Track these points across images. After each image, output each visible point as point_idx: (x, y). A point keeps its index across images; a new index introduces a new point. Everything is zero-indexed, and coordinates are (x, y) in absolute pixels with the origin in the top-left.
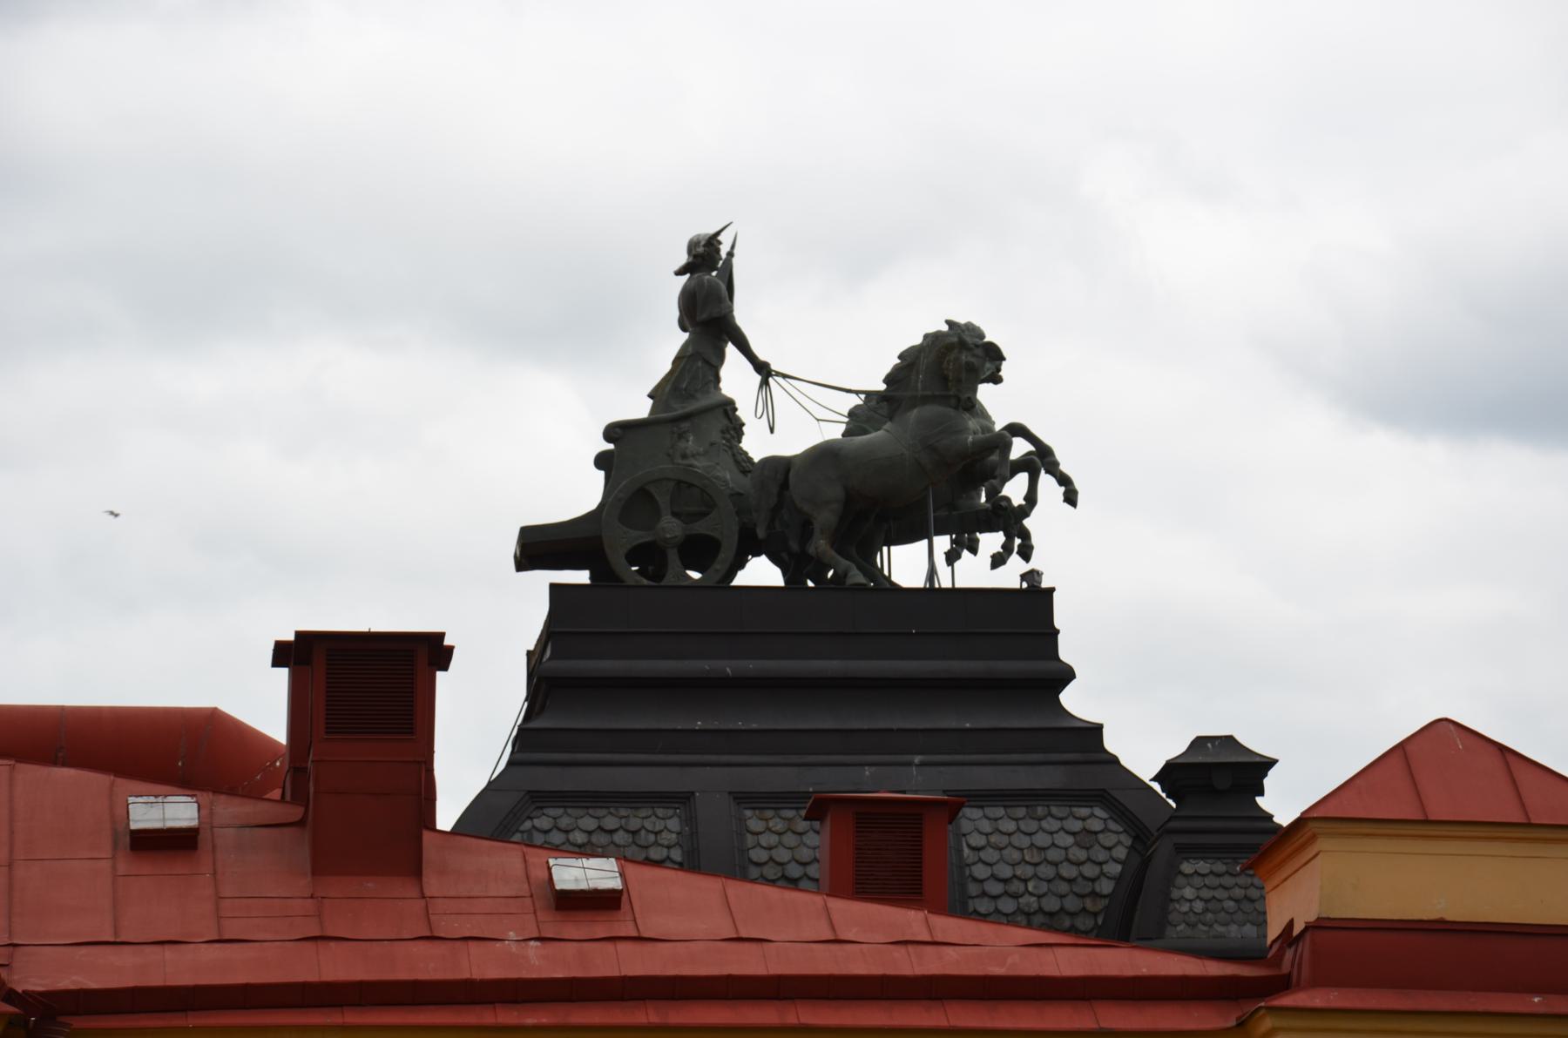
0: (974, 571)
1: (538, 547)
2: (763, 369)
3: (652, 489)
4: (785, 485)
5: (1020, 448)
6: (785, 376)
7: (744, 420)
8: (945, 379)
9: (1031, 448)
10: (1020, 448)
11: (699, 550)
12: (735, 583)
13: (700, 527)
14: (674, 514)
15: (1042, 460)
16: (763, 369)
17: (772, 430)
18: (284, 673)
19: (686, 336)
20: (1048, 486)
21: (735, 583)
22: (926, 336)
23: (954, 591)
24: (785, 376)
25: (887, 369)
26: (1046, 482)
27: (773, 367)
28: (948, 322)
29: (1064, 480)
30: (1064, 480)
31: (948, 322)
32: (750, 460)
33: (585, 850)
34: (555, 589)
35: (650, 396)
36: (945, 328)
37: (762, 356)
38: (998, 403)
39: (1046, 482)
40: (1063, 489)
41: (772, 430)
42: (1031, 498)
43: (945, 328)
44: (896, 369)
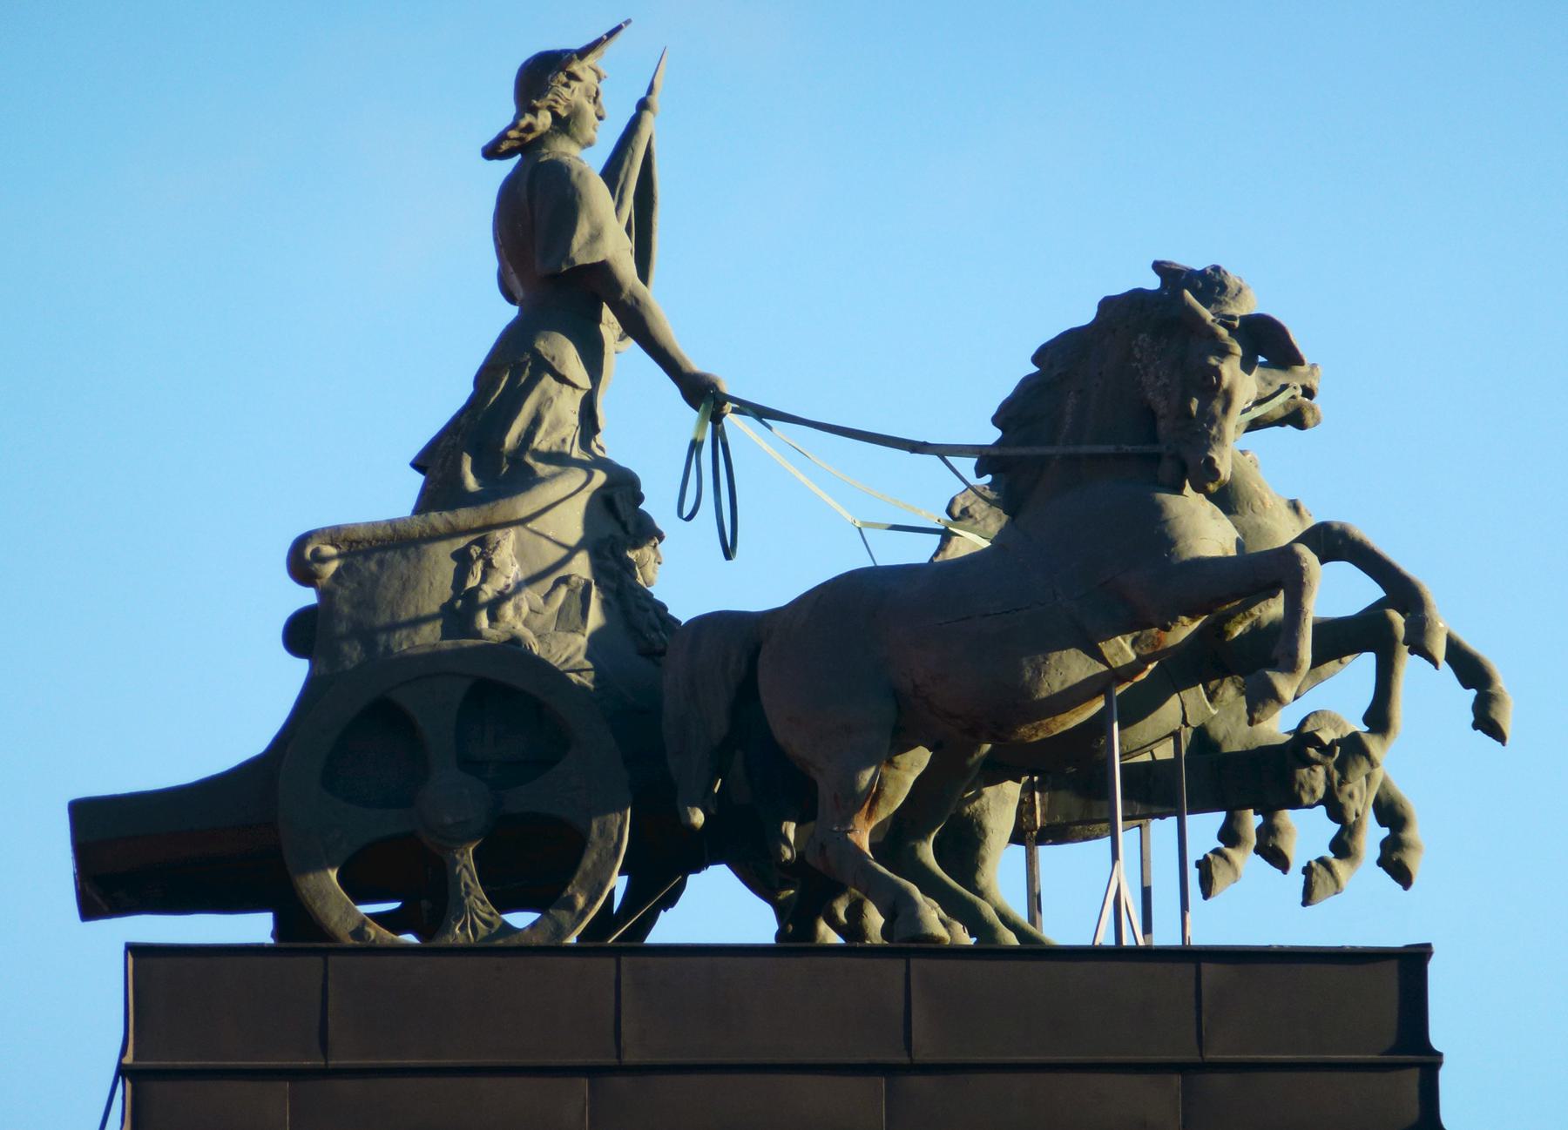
0: (1255, 909)
1: (127, 852)
2: (701, 392)
4: (747, 692)
5: (1337, 591)
6: (762, 414)
8: (1150, 415)
11: (535, 863)
12: (655, 937)
15: (1393, 623)
16: (701, 392)
17: (729, 553)
18: (299, 669)
20: (1425, 687)
21: (655, 937)
22: (1107, 304)
23: (1187, 955)
24: (762, 414)
25: (1005, 389)
27: (727, 388)
28: (1159, 267)
29: (1470, 669)
30: (1470, 669)
31: (1159, 267)
32: (677, 622)
34: (136, 951)
35: (418, 465)
36: (1153, 282)
37: (697, 362)
38: (1272, 476)
40: (1473, 692)
41: (729, 553)
42: (1379, 717)
43: (1153, 282)
44: (1027, 387)
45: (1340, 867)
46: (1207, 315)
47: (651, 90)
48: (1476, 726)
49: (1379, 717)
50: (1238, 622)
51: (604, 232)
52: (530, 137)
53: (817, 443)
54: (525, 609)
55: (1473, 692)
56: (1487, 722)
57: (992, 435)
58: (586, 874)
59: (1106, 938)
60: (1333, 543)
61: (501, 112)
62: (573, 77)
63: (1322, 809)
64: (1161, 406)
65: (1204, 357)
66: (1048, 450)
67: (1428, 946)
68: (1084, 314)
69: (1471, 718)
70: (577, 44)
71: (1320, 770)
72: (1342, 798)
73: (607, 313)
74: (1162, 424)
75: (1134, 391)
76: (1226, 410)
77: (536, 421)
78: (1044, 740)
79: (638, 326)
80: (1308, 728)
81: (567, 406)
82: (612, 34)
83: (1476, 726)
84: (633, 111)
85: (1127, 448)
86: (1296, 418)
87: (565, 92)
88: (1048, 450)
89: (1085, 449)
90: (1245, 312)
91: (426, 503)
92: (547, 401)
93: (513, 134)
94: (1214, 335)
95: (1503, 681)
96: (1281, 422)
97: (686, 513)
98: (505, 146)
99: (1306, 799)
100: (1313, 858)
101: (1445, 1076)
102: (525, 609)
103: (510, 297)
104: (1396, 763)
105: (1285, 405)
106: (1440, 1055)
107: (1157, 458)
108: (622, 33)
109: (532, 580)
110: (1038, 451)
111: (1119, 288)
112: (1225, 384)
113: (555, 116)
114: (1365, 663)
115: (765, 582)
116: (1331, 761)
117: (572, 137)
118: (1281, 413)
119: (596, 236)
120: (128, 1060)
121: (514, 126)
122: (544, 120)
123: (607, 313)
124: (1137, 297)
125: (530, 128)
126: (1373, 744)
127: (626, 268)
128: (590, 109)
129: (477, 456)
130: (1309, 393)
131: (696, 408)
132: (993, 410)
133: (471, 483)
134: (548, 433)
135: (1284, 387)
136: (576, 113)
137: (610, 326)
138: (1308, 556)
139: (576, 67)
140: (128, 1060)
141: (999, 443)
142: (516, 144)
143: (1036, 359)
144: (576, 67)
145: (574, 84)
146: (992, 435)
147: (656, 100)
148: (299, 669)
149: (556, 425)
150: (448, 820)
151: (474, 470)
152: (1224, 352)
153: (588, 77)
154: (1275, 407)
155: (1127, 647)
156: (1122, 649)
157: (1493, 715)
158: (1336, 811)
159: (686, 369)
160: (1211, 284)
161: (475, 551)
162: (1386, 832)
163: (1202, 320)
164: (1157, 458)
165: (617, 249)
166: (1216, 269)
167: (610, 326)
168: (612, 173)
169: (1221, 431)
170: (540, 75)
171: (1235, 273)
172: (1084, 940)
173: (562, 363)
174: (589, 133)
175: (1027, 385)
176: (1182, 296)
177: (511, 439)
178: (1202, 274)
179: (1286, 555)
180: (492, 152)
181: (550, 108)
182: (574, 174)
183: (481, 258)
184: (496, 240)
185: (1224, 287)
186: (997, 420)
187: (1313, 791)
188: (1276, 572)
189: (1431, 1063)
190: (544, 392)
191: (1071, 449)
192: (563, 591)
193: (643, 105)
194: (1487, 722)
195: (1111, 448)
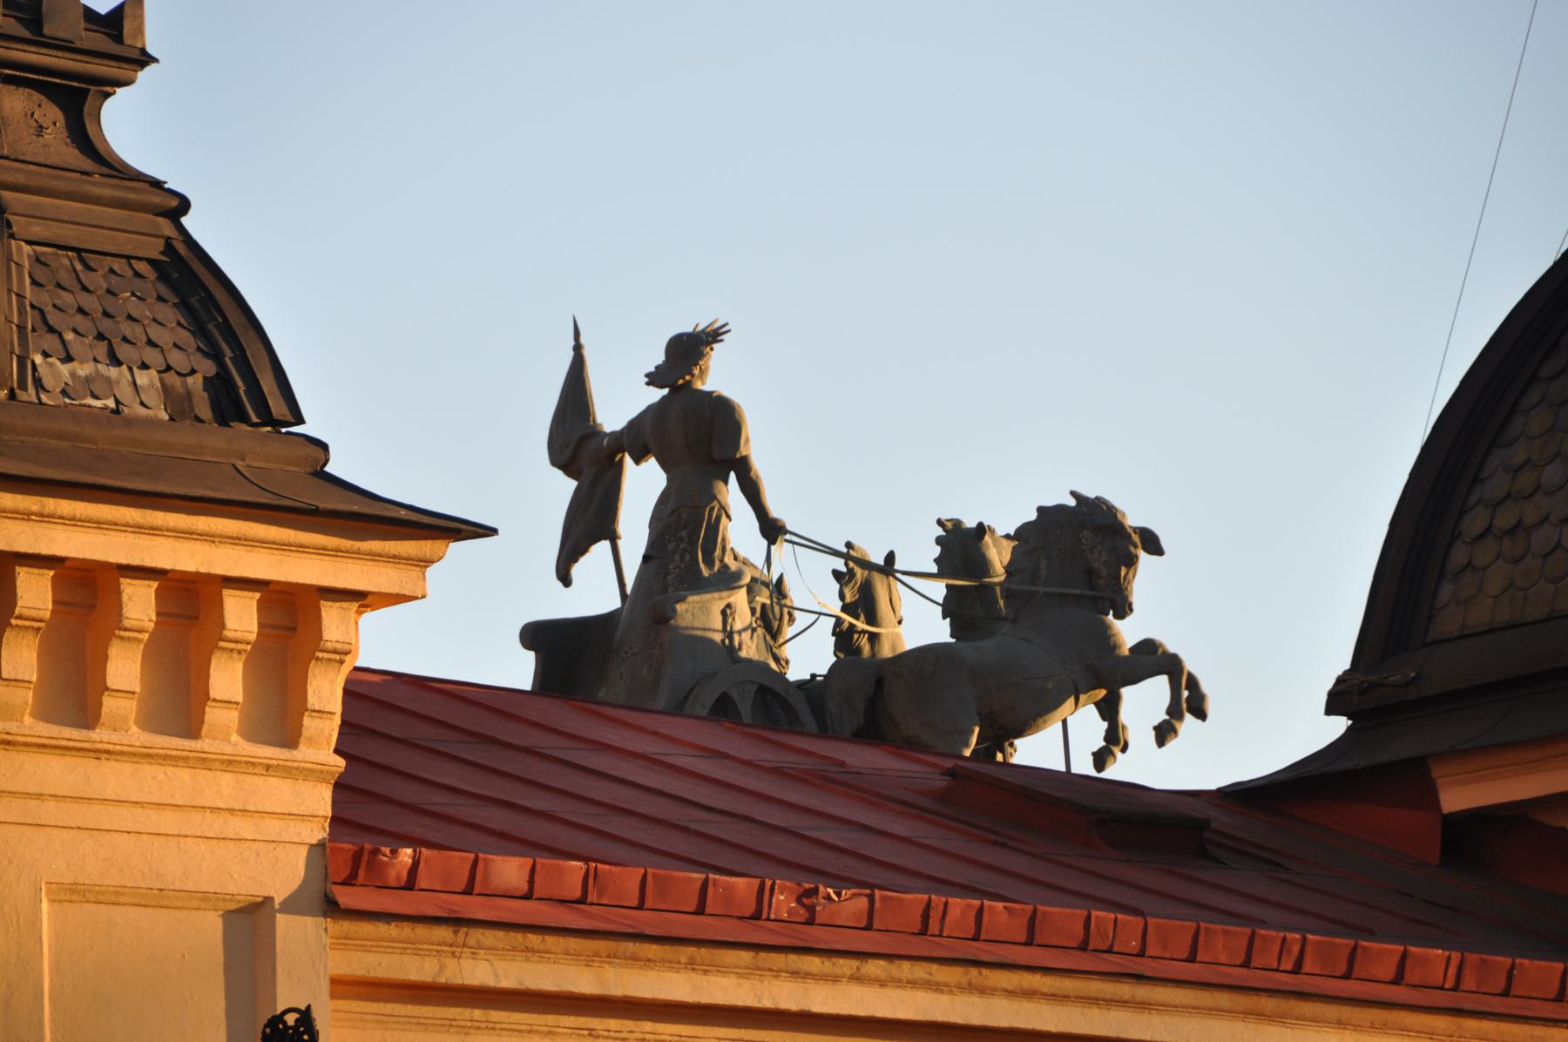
8: (1090, 574)
31: (1073, 494)
36: (1072, 502)
37: (775, 510)
40: (1105, 725)
89: (1053, 590)
111: (1050, 502)
124: (1060, 509)
152: (1136, 547)
164: (1093, 599)
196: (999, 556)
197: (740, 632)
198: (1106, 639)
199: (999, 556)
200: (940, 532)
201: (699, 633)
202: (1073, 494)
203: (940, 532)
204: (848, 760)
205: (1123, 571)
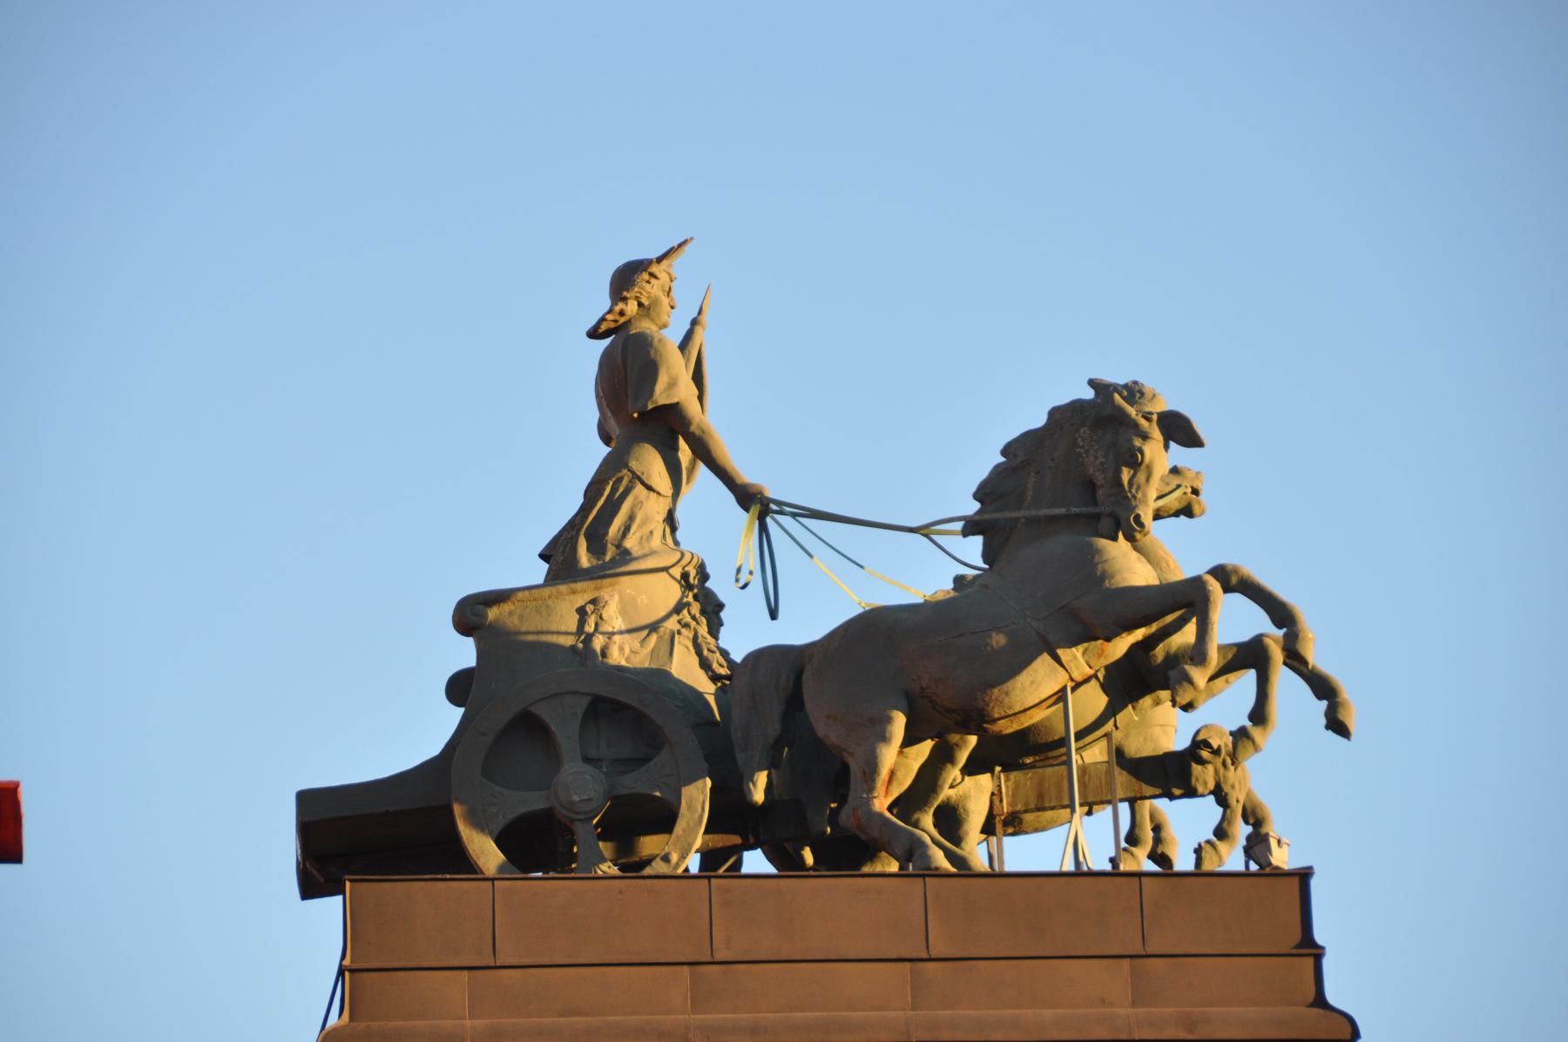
2: (747, 496)
3: (545, 712)
4: (794, 702)
5: (1235, 620)
7: (722, 597)
8: (1091, 486)
9: (1060, 652)
10: (1235, 620)
13: (632, 783)
14: (587, 760)
16: (747, 496)
17: (774, 615)
18: (454, 715)
19: (606, 450)
22: (1055, 413)
25: (983, 473)
26: (1287, 685)
27: (771, 493)
28: (1092, 383)
29: (1322, 687)
30: (1322, 687)
31: (1092, 383)
33: (769, 789)
35: (544, 556)
36: (1089, 394)
37: (747, 474)
39: (1285, 681)
40: (1324, 703)
41: (774, 615)
42: (1259, 715)
43: (1089, 394)
45: (1221, 845)
46: (1132, 411)
47: (700, 312)
48: (1328, 727)
49: (1259, 715)
50: (1152, 647)
51: (674, 385)
52: (622, 320)
53: (841, 516)
54: (627, 650)
55: (1324, 703)
56: (1337, 725)
57: (973, 507)
58: (678, 838)
59: (1069, 866)
60: (1230, 580)
61: (599, 303)
62: (652, 275)
63: (1212, 798)
64: (1099, 478)
65: (1130, 440)
66: (1015, 514)
67: (1310, 868)
68: (1039, 420)
69: (1324, 721)
70: (654, 255)
71: (1210, 768)
72: (1226, 788)
73: (682, 443)
74: (1100, 493)
75: (1074, 474)
76: (1148, 480)
77: (631, 518)
78: (1017, 733)
79: (704, 452)
80: (1201, 737)
81: (654, 508)
82: (680, 245)
83: (1328, 727)
84: (688, 327)
85: (1075, 510)
86: (1187, 511)
87: (648, 287)
88: (1015, 514)
89: (1044, 512)
90: (1159, 410)
91: (552, 578)
92: (638, 504)
93: (610, 317)
94: (1136, 425)
95: (1348, 690)
96: (1177, 514)
97: (741, 583)
98: (604, 327)
99: (1200, 790)
100: (1202, 840)
101: (1327, 963)
102: (627, 650)
103: (606, 439)
104: (1257, 776)
105: (1179, 499)
106: (1322, 948)
107: (1096, 517)
108: (687, 248)
109: (630, 631)
110: (1008, 514)
111: (1063, 399)
112: (1147, 459)
113: (640, 305)
114: (1249, 677)
115: (804, 625)
116: (1219, 761)
117: (652, 320)
118: (1176, 506)
119: (673, 384)
120: (347, 962)
121: (610, 311)
122: (631, 308)
123: (682, 443)
124: (1077, 406)
125: (622, 313)
126: (1256, 733)
127: (692, 407)
128: (665, 300)
129: (586, 546)
130: (1195, 492)
131: (747, 510)
132: (974, 488)
133: (584, 559)
134: (640, 527)
135: (1179, 486)
136: (655, 302)
137: (685, 453)
138: (1214, 586)
139: (654, 269)
140: (347, 962)
141: (978, 513)
142: (613, 325)
143: (1004, 452)
144: (654, 269)
145: (653, 281)
146: (973, 507)
147: (705, 318)
148: (454, 715)
149: (644, 522)
150: (576, 798)
151: (589, 549)
152: (1145, 437)
153: (664, 277)
154: (1173, 501)
155: (1079, 655)
156: (1075, 657)
157: (1341, 717)
158: (1221, 798)
159: (739, 481)
160: (1133, 392)
161: (590, 608)
162: (1249, 829)
163: (1128, 416)
164: (1096, 517)
165: (685, 393)
166: (1136, 383)
167: (685, 453)
168: (684, 346)
169: (1145, 495)
170: (625, 278)
171: (1148, 383)
172: (1055, 868)
173: (649, 476)
174: (664, 318)
175: (997, 470)
176: (1113, 400)
177: (614, 529)
178: (1126, 386)
179: (1197, 583)
180: (594, 334)
181: (637, 298)
182: (656, 342)
183: (589, 412)
184: (597, 396)
185: (1142, 394)
186: (976, 496)
187: (1206, 783)
188: (1189, 600)
189: (1317, 954)
190: (636, 498)
191: (1033, 513)
192: (654, 637)
193: (694, 322)
194: (1337, 725)
195: (1062, 511)
196: (1137, 442)
197: (610, 635)
198: (1091, 572)
199: (1137, 442)
200: (465, 654)
201: (530, 638)
202: (1092, 383)
203: (465, 654)
204: (1112, 980)
205: (1126, 475)
